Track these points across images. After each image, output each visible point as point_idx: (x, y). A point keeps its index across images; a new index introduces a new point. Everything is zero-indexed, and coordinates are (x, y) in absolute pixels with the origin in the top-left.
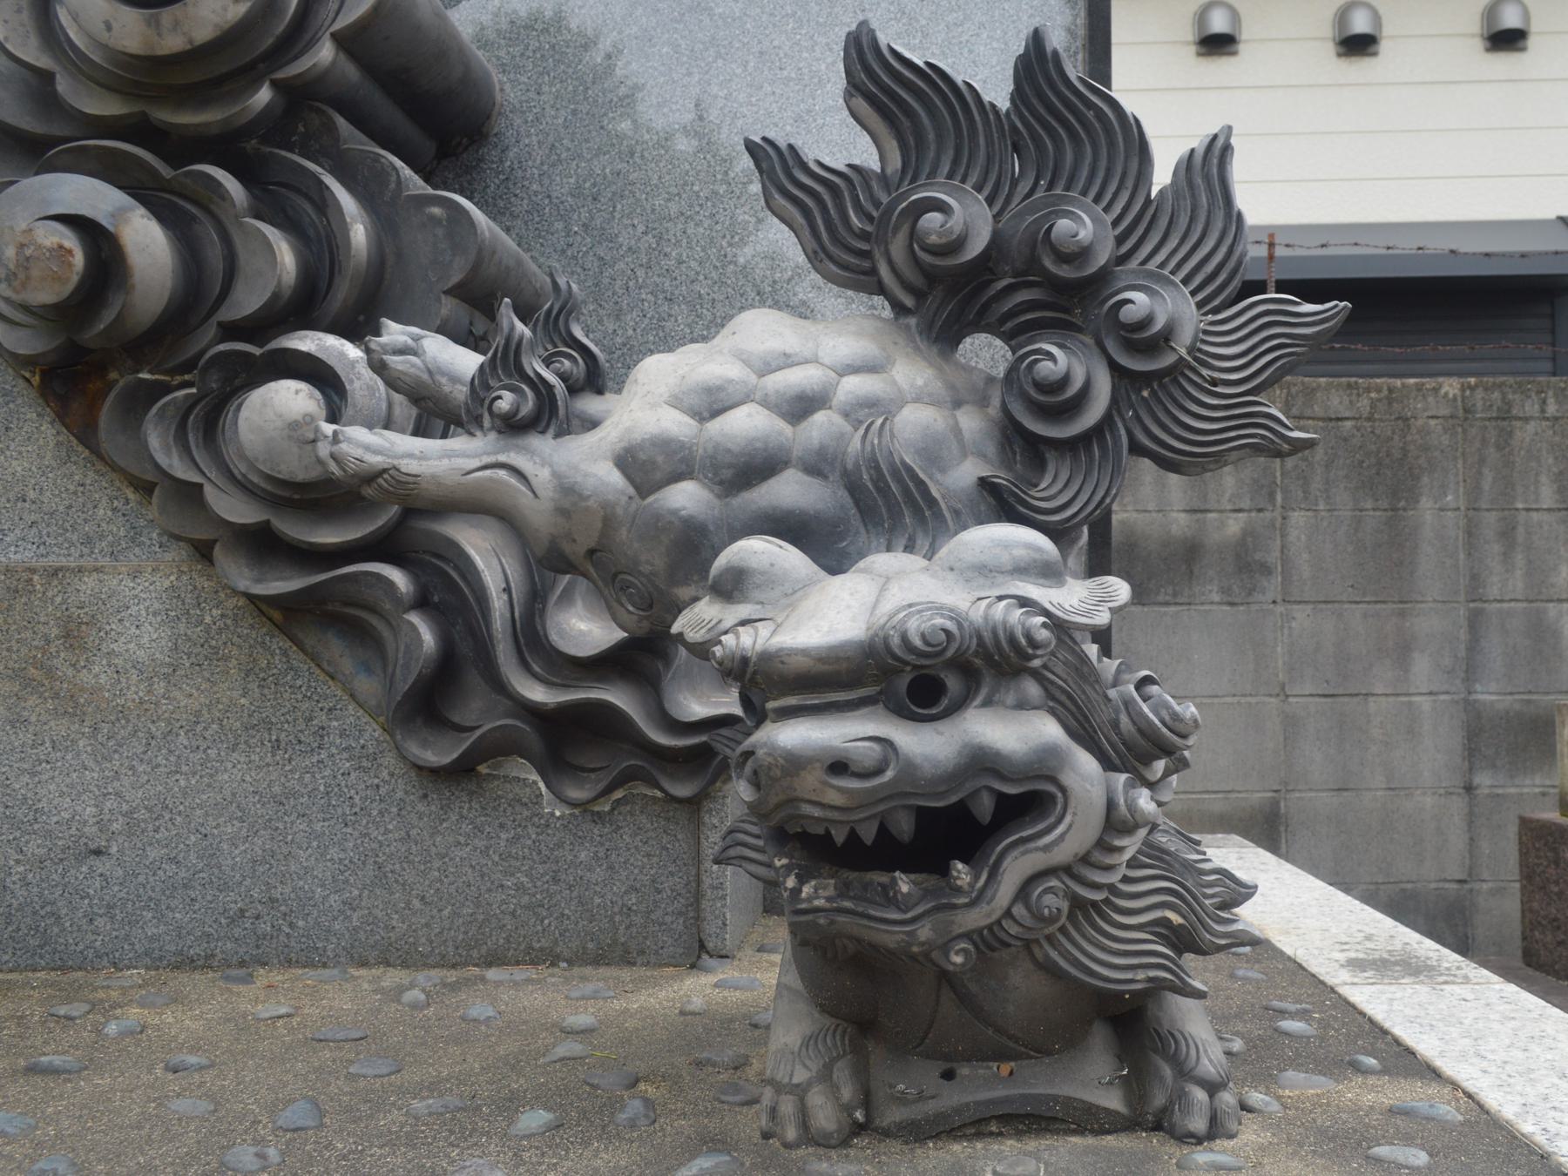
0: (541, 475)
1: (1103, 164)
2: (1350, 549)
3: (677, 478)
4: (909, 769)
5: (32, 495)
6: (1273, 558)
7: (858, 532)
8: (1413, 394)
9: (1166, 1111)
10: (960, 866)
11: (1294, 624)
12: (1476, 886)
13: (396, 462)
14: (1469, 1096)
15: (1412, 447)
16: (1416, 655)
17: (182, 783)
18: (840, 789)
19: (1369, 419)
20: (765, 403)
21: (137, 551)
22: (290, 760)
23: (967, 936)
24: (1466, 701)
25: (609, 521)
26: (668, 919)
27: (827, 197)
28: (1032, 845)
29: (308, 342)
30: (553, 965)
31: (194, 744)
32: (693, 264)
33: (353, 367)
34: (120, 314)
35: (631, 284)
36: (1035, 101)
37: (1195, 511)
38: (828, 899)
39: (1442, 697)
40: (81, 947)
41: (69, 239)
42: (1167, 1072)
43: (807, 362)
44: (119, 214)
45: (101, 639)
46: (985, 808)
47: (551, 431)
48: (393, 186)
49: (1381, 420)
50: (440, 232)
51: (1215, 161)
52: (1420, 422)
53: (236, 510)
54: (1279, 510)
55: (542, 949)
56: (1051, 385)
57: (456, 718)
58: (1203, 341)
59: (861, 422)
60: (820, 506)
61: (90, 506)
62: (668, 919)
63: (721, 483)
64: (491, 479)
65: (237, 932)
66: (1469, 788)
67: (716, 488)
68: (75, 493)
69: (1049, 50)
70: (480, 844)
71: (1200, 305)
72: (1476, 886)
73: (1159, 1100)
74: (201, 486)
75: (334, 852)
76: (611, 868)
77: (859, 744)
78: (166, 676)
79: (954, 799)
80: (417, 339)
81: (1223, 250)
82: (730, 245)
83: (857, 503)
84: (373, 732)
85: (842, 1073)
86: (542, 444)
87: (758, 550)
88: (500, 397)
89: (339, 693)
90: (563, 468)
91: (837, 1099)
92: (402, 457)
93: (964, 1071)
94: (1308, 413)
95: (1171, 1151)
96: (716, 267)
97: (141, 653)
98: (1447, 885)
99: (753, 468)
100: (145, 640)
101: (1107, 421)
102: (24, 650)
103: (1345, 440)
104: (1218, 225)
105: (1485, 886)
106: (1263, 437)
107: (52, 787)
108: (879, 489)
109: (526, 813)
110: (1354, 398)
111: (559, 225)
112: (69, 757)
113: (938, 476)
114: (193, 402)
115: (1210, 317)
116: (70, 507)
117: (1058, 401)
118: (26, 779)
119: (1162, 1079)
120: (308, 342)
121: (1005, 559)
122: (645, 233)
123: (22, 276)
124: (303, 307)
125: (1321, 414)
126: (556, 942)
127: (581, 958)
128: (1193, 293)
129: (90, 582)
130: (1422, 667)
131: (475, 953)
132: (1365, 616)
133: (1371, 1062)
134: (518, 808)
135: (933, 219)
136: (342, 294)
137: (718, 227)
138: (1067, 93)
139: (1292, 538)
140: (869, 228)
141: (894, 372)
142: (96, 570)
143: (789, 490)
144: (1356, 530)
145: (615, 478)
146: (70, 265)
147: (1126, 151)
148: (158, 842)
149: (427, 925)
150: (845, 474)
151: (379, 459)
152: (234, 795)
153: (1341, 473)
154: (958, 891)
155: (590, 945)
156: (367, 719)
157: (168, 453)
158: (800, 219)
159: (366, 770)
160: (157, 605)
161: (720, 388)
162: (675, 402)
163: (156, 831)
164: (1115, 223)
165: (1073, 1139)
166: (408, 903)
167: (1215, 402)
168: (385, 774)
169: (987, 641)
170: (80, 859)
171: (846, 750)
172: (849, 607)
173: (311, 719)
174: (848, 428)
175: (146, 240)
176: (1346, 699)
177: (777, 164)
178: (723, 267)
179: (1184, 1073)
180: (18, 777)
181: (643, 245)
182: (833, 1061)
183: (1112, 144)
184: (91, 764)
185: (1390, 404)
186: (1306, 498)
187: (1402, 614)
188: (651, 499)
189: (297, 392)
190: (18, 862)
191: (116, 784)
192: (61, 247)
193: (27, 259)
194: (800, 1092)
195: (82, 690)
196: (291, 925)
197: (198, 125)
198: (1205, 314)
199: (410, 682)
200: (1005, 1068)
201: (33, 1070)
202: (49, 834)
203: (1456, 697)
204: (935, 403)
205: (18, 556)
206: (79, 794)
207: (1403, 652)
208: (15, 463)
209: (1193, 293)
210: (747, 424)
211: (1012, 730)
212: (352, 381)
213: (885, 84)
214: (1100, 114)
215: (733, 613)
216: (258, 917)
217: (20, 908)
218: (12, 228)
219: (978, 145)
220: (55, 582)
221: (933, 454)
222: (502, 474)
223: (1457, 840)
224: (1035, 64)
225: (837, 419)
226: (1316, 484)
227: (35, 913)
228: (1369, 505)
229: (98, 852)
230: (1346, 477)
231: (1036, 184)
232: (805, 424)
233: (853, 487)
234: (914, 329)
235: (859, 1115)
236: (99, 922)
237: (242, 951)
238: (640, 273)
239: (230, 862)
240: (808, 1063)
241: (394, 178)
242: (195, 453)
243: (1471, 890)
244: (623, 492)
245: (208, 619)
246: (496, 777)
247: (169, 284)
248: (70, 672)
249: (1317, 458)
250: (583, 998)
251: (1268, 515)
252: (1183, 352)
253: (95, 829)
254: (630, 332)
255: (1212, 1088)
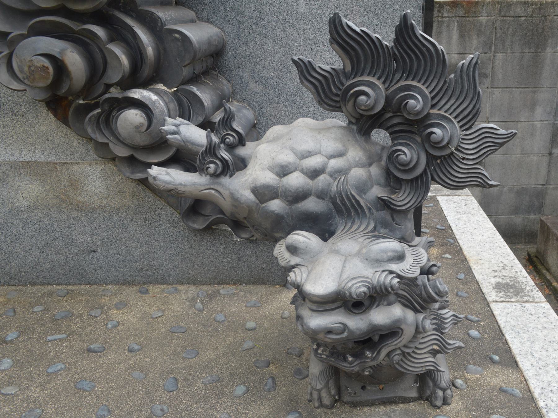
0: (226, 193)
1: (428, 68)
2: (518, 68)
3: (273, 198)
4: (351, 332)
5: (50, 138)
6: (489, 71)
7: (335, 217)
8: (549, 6)
9: (430, 396)
10: (368, 353)
11: (494, 96)
12: (548, 186)
13: (176, 187)
14: (526, 381)
15: (546, 28)
16: (538, 107)
17: (117, 231)
18: (330, 338)
19: (531, 17)
20: (302, 171)
21: (89, 157)
22: (150, 224)
23: (371, 367)
24: (553, 124)
25: (250, 211)
26: (276, 271)
27: (323, 81)
28: (391, 344)
29: (137, 94)
30: (241, 284)
31: (119, 219)
32: (273, 23)
33: (155, 104)
34: (69, 87)
35: (251, 31)
36: (403, 44)
37: (461, 54)
38: (327, 356)
39: (545, 122)
40: (94, 278)
41: (46, 63)
42: (431, 384)
43: (317, 154)
44: (62, 52)
45: (83, 186)
46: (376, 338)
47: (228, 175)
48: (160, 24)
49: (536, 17)
50: (179, 44)
51: (472, 69)
52: (551, 18)
53: (122, 152)
54: (493, 53)
55: (237, 280)
56: (405, 163)
57: (203, 213)
58: (461, 142)
59: (336, 178)
60: (322, 210)
61: (70, 142)
62: (276, 271)
63: (288, 201)
64: (209, 193)
65: (141, 274)
66: (550, 154)
67: (287, 203)
68: (65, 137)
69: (409, 23)
70: (215, 249)
71: (461, 127)
72: (548, 186)
73: (428, 393)
74: (108, 144)
75: (168, 251)
76: (257, 256)
77: (336, 325)
78: (106, 198)
79: (366, 338)
80: (177, 126)
81: (471, 106)
82: (287, 15)
83: (335, 208)
84: (176, 216)
85: (331, 384)
86: (225, 180)
87: (302, 238)
88: (209, 167)
89: (164, 203)
90: (234, 191)
91: (330, 393)
92: (178, 185)
93: (369, 388)
94: (508, 14)
95: (430, 410)
96: (282, 24)
97: (96, 190)
98: (538, 186)
99: (299, 196)
100: (97, 186)
101: (425, 171)
102: (58, 190)
103: (521, 25)
104: (471, 96)
105: (551, 187)
106: (480, 182)
107: (76, 232)
108: (342, 204)
109: (228, 240)
110: (526, 8)
111: (222, 8)
112: (79, 223)
113: (363, 196)
114: (99, 115)
115: (464, 133)
116: (64, 142)
117: (407, 168)
118: (67, 229)
119: (429, 387)
120: (137, 94)
121: (385, 257)
122: (255, 11)
123: (32, 77)
124: (135, 79)
125: (513, 15)
126: (241, 278)
127: (249, 282)
128: (458, 122)
129: (75, 168)
130: (539, 111)
131: (216, 281)
132: (521, 93)
133: (497, 358)
134: (226, 239)
135: (363, 98)
136: (146, 71)
137: (282, 8)
138: (416, 41)
139: (496, 64)
140: (339, 93)
141: (348, 155)
142: (77, 163)
143: (312, 205)
144: (521, 61)
145: (252, 197)
146: (49, 73)
147: (437, 62)
148: (112, 248)
149: (200, 273)
150: (331, 198)
151: (170, 186)
152: (134, 234)
153: (518, 38)
154: (368, 357)
155: (252, 279)
156: (174, 211)
157: (95, 134)
158: (313, 90)
159: (175, 227)
160: (99, 175)
161: (287, 166)
162: (271, 169)
163: (111, 245)
164: (433, 98)
165: (401, 405)
166: (194, 266)
167: (464, 167)
168: (182, 228)
169: (378, 290)
170: (89, 253)
171: (332, 327)
172: (332, 275)
173: (155, 211)
174: (332, 181)
175: (74, 60)
176: (510, 123)
177: (305, 70)
178: (285, 24)
179: (436, 385)
180: (64, 229)
181: (254, 16)
182: (329, 380)
183: (432, 61)
184: (87, 225)
185: (540, 10)
186: (503, 48)
187: (534, 92)
188: (264, 205)
189: (136, 115)
190: (69, 254)
191: (96, 231)
192: (44, 66)
193: (33, 71)
194: (319, 391)
195: (80, 202)
196: (158, 272)
197: (84, 10)
198: (463, 131)
199: (187, 206)
200: (381, 387)
201: (89, 351)
202: (78, 246)
203: (550, 122)
204: (363, 166)
205: (50, 159)
206: (85, 234)
207: (532, 107)
208: (42, 127)
209: (458, 122)
210: (296, 180)
211: (380, 316)
212: (155, 110)
213: (340, 36)
214: (428, 49)
215: (294, 260)
216: (147, 270)
217: (73, 267)
218: (25, 60)
219: (380, 61)
220: (64, 168)
221: (362, 188)
222: (213, 191)
223: (543, 171)
224: (404, 29)
225: (328, 178)
226: (508, 43)
227: (78, 269)
228: (527, 51)
229: (94, 251)
230: (520, 40)
231: (402, 75)
232: (316, 180)
233: (334, 203)
234: (355, 131)
235: (337, 398)
236: (98, 271)
237: (143, 280)
238: (254, 27)
239: (136, 254)
240: (321, 382)
241: (160, 22)
242: (103, 130)
243: (546, 188)
244: (254, 202)
245: (117, 180)
246: (218, 229)
247: (85, 75)
248: (75, 197)
249: (509, 33)
250: (251, 307)
251: (488, 55)
252: (453, 149)
253: (92, 244)
254: (252, 50)
255: (444, 390)
